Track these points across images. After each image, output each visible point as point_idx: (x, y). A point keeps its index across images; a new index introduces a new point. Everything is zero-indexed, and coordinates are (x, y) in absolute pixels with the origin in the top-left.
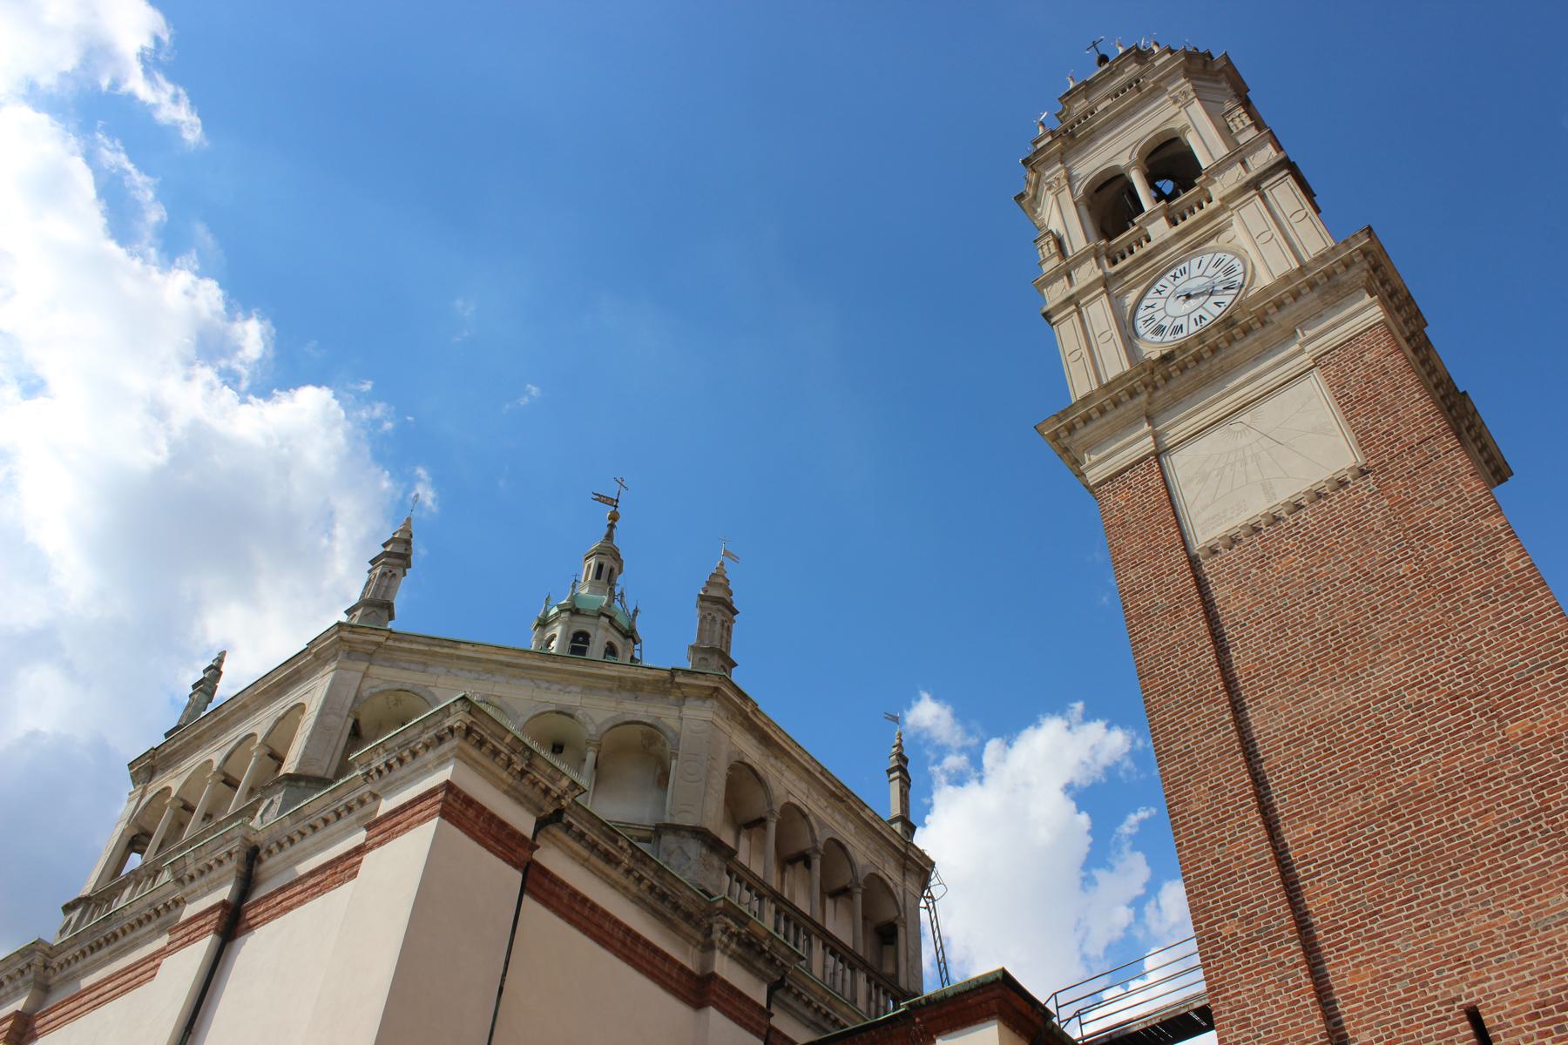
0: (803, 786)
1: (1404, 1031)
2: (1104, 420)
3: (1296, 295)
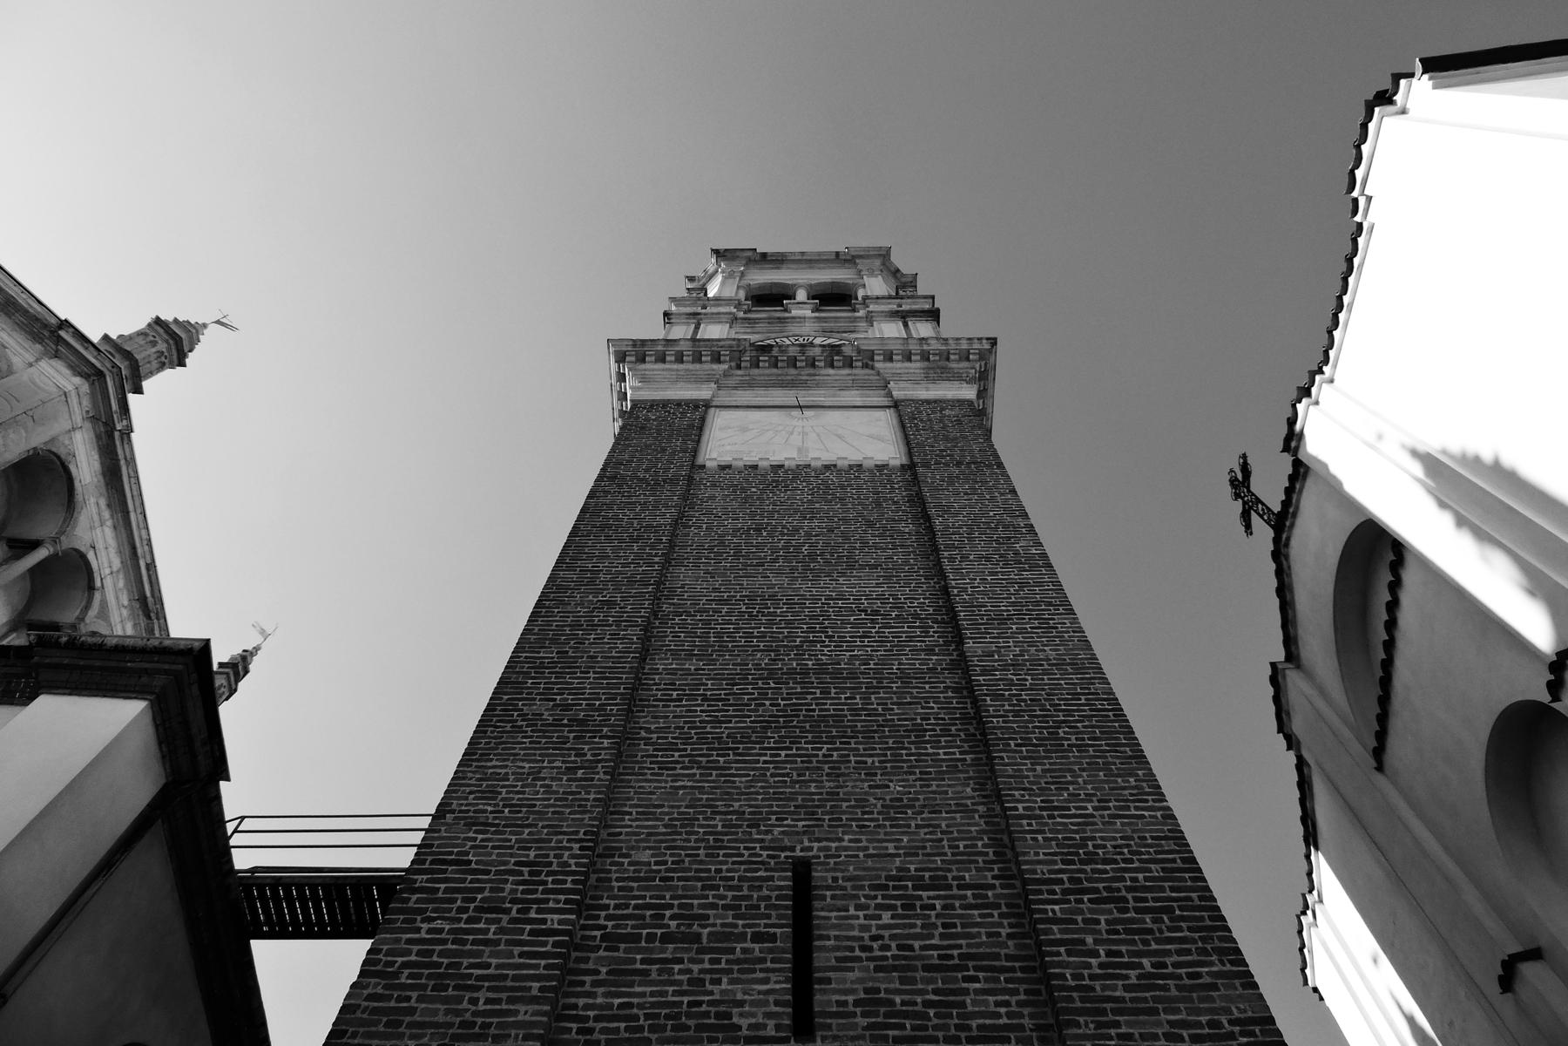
0: (117, 563)
1: (701, 862)
2: (675, 366)
3: (908, 357)
